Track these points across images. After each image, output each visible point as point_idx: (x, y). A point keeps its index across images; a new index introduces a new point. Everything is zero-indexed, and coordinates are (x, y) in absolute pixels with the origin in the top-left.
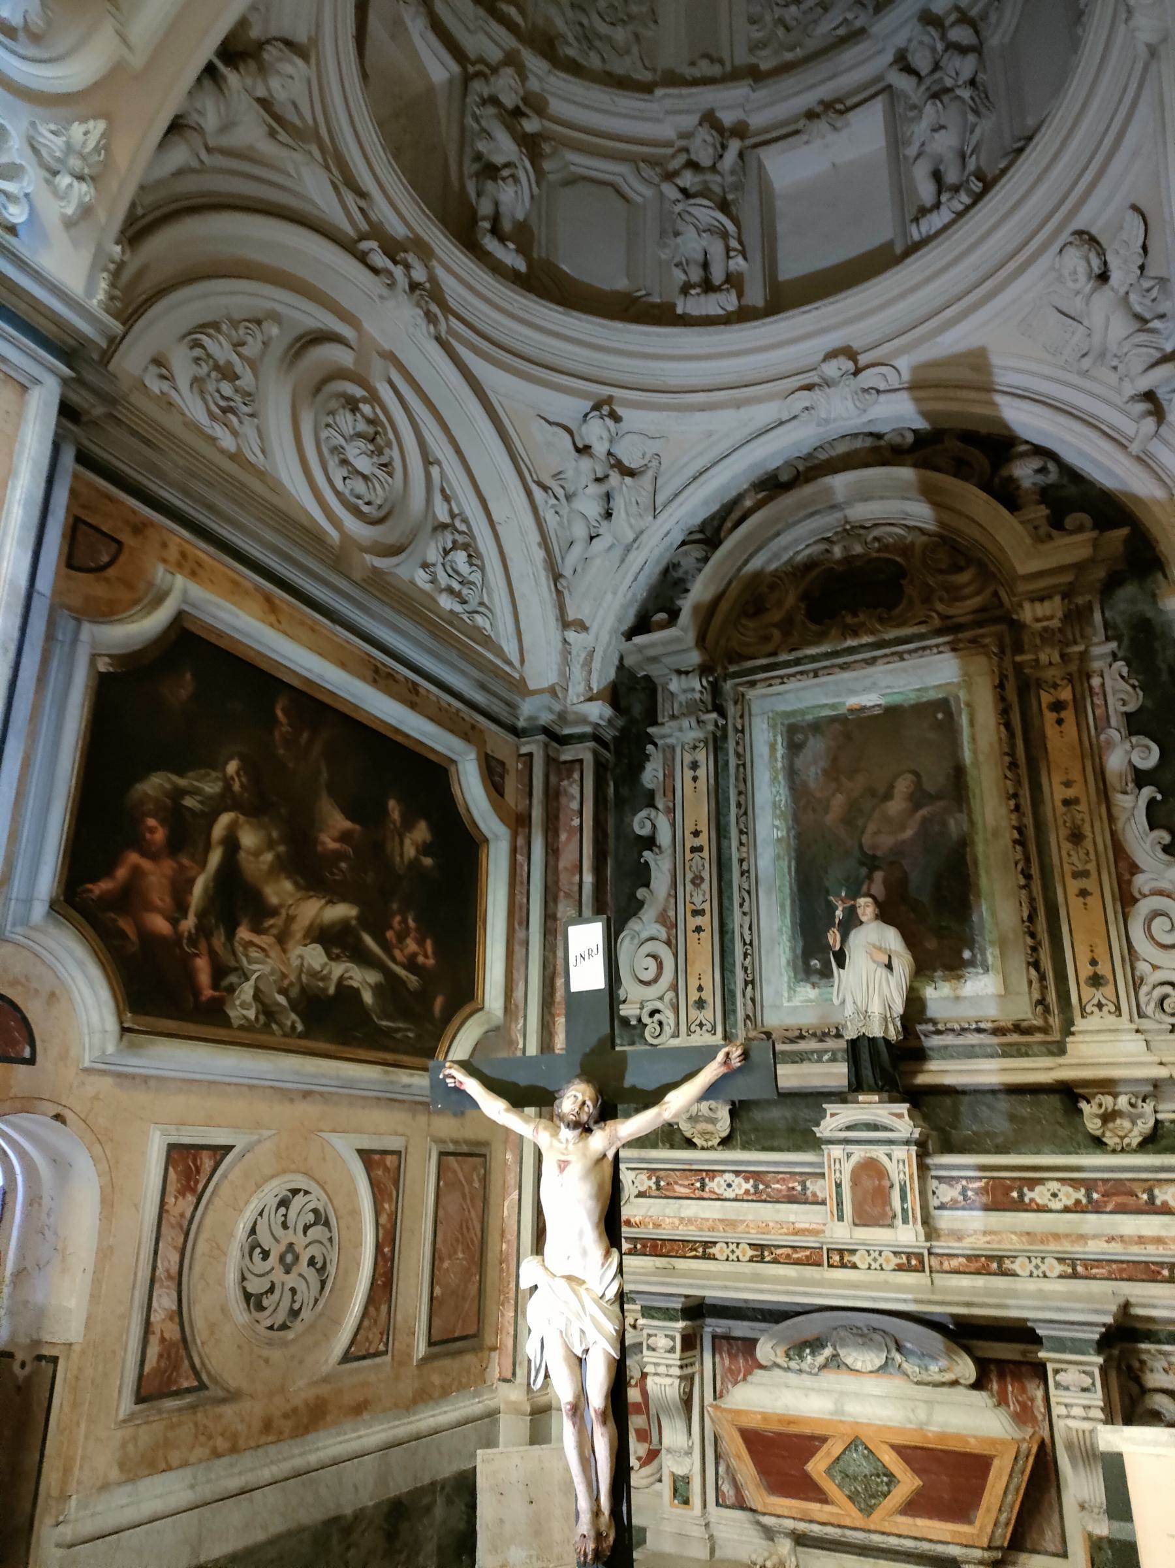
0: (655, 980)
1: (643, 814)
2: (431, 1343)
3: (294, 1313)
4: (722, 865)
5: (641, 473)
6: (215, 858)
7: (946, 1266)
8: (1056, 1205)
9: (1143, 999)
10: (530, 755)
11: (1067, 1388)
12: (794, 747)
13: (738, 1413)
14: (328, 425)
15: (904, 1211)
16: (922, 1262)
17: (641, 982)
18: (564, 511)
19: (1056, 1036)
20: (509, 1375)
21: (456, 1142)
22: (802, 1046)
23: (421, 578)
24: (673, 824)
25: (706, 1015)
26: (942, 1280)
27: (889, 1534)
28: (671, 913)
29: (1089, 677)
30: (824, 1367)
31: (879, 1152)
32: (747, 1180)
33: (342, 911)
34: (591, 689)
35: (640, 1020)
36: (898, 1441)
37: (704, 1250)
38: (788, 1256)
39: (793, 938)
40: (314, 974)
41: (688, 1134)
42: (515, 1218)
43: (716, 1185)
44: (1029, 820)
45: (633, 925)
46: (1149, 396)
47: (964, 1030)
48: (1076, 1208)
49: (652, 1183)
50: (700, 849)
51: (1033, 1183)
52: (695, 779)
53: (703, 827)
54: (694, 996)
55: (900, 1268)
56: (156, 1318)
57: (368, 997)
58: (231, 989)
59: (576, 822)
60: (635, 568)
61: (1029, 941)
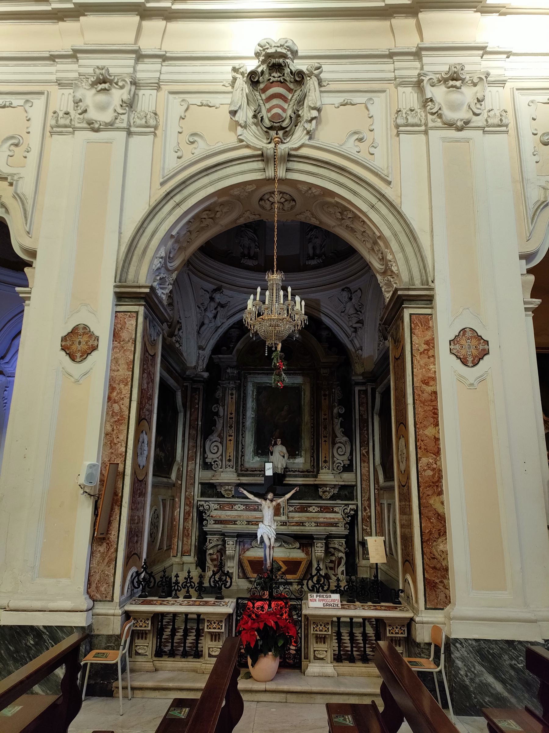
0: (216, 453)
1: (215, 405)
4: (238, 423)
5: (226, 306)
7: (291, 525)
8: (314, 511)
9: (334, 466)
10: (187, 386)
12: (259, 393)
15: (283, 513)
17: (212, 453)
19: (315, 473)
20: (176, 555)
22: (255, 472)
24: (224, 410)
25: (231, 463)
26: (290, 527)
28: (222, 435)
29: (332, 389)
32: (244, 506)
35: (211, 463)
37: (234, 522)
39: (254, 444)
41: (223, 494)
43: (236, 507)
45: (211, 437)
46: (355, 328)
47: (295, 471)
50: (232, 418)
52: (232, 398)
53: (234, 412)
55: (281, 525)
61: (312, 451)
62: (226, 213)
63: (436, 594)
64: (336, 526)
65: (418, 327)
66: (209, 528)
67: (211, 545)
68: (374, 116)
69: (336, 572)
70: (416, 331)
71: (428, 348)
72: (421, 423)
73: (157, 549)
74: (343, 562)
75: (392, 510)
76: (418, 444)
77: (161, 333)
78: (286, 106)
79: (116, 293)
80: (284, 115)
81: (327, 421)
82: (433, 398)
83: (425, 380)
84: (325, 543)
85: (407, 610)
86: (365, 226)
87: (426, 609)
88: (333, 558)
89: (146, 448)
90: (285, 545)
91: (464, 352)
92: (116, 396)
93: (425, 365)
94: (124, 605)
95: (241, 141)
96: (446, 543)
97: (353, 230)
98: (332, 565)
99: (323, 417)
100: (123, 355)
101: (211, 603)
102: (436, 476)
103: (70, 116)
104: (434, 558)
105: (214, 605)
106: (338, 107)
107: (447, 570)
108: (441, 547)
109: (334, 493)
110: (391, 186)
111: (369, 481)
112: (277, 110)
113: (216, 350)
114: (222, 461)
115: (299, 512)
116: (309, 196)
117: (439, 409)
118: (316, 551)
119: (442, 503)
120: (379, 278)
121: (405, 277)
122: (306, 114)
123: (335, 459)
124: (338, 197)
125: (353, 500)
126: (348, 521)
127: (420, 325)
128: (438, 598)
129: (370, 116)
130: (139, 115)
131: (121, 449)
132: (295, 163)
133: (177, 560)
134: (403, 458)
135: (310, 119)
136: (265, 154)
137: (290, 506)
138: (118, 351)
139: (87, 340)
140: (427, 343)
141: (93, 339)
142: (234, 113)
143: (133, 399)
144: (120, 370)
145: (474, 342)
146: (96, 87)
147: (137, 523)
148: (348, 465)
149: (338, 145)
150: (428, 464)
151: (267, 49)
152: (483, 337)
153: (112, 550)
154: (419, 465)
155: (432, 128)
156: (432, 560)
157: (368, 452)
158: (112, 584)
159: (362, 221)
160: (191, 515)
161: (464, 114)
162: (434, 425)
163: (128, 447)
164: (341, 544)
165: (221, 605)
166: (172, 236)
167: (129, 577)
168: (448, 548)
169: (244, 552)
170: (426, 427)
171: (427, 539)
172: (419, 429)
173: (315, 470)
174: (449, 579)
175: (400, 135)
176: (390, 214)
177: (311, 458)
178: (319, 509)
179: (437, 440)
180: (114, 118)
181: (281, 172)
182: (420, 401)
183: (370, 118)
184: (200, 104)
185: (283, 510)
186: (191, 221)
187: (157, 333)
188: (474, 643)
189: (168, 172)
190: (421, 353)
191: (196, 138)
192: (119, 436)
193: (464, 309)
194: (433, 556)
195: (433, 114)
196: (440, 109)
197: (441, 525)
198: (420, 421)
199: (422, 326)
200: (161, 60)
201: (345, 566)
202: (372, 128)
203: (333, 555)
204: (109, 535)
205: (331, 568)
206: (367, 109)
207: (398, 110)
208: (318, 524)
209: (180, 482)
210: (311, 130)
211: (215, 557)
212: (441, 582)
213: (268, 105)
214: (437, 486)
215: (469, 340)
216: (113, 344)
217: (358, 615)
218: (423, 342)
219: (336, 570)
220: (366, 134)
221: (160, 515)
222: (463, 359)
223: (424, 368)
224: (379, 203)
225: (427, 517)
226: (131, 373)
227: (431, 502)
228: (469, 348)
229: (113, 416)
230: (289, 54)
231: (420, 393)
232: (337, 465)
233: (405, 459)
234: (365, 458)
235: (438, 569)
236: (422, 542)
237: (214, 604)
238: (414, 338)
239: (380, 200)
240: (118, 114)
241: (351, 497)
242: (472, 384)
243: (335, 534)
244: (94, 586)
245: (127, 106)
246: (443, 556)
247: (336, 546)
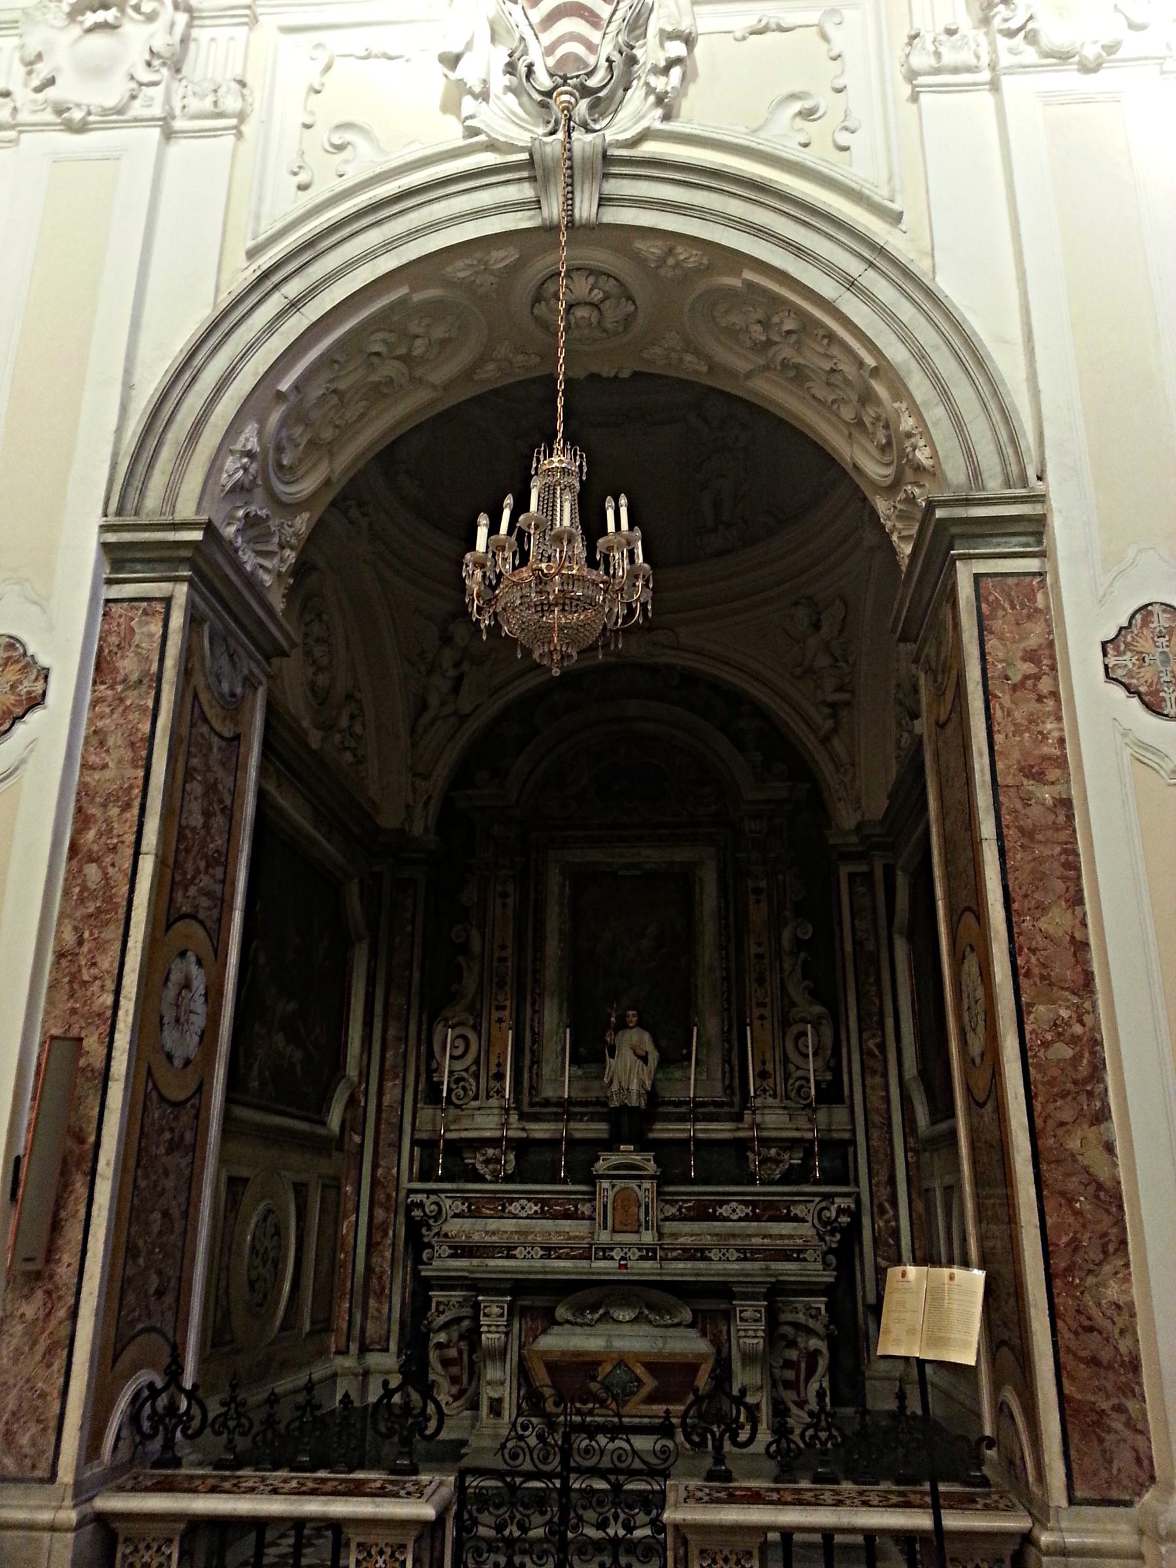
2: (313, 1322)
7: (670, 1256)
8: (735, 1217)
9: (789, 1088)
11: (746, 1321)
13: (545, 1352)
15: (647, 1222)
16: (655, 1254)
19: (736, 1110)
27: (634, 1416)
28: (478, 1006)
30: (599, 1320)
31: (633, 1184)
36: (648, 1359)
38: (567, 1254)
42: (352, 1234)
44: (733, 965)
48: (746, 1218)
49: (465, 1207)
50: (504, 960)
51: (721, 1203)
52: (504, 905)
54: (494, 1070)
61: (726, 1046)
62: (443, 343)
63: (1104, 1451)
64: (798, 1259)
65: (1000, 613)
66: (437, 1270)
67: (442, 1319)
68: (847, 56)
69: (802, 1395)
70: (997, 625)
71: (1036, 670)
72: (1026, 896)
73: (276, 1330)
74: (823, 1364)
75: (955, 1213)
77: (261, 683)
78: (595, 36)
79: (105, 547)
80: (592, 60)
81: (766, 961)
82: (1062, 819)
83: (1032, 767)
84: (767, 1309)
85: (1009, 1508)
86: (835, 351)
87: (1072, 1501)
88: (793, 1355)
89: (199, 1005)
90: (651, 1317)
91: (1148, 676)
92: (94, 842)
93: (1030, 722)
94: (90, 1494)
95: (473, 132)
96: (1127, 1279)
97: (798, 376)
98: (790, 1375)
99: (754, 950)
100: (122, 721)
101: (373, 1485)
102: (1085, 1061)
103: (14, 101)
104: (1091, 1329)
105: (381, 1493)
106: (744, 38)
107: (1134, 1366)
108: (1112, 1291)
109: (791, 1165)
110: (903, 227)
111: (890, 1126)
113: (461, 777)
114: (477, 1076)
115: (691, 1219)
116: (669, 275)
117: (1081, 851)
118: (742, 1333)
119: (1109, 1148)
120: (882, 505)
121: (955, 472)
122: (650, 52)
123: (792, 1068)
124: (752, 269)
125: (846, 1183)
126: (834, 1245)
127: (1007, 606)
128: (1110, 1462)
129: (834, 53)
130: (197, 89)
131: (101, 1000)
133: (348, 1362)
134: (977, 1015)
135: (662, 64)
136: (536, 157)
137: (666, 1202)
138: (108, 710)
139: (14, 678)
140: (1031, 656)
141: (33, 677)
142: (452, 61)
143: (144, 848)
144: (111, 764)
146: (80, 18)
147: (160, 1234)
148: (829, 1083)
149: (745, 130)
150: (1055, 1025)
153: (62, 1313)
155: (1011, 70)
157: (882, 1046)
158: (53, 1424)
159: (824, 337)
160: (391, 1233)
162: (1067, 901)
163: (124, 992)
164: (814, 1312)
165: (402, 1493)
166: (280, 396)
167: (123, 1402)
168: (1134, 1291)
169: (536, 1337)
170: (1042, 909)
171: (1063, 1265)
172: (1019, 915)
173: (737, 1099)
174: (1144, 1397)
175: (922, 96)
176: (904, 300)
177: (723, 1066)
178: (749, 1210)
179: (1080, 947)
180: (127, 95)
181: (586, 205)
183: (834, 59)
184: (364, 53)
185: (647, 1214)
186: (337, 357)
187: (246, 679)
189: (267, 229)
190: (1014, 688)
191: (348, 136)
192: (98, 959)
193: (1140, 551)
194: (1086, 1323)
195: (1011, 34)
197: (1107, 1220)
198: (1023, 891)
199: (1013, 607)
201: (827, 1377)
202: (839, 84)
203: (792, 1344)
204: (53, 1266)
205: (788, 1385)
206: (825, 37)
207: (913, 33)
208: (746, 1254)
209: (357, 1139)
210: (666, 92)
211: (453, 1353)
212: (1120, 1409)
213: (548, 38)
214: (1090, 1094)
215: (1161, 639)
216: (94, 691)
217: (846, 1526)
219: (802, 1389)
220: (824, 100)
221: (287, 1228)
222: (1147, 694)
223: (1028, 729)
224: (871, 273)
226: (142, 774)
227: (1073, 1144)
229: (82, 900)
232: (798, 1083)
233: (981, 1017)
234: (874, 1064)
235: (1105, 1363)
237: (382, 1488)
238: (992, 643)
239: (871, 264)
240: (141, 84)
241: (841, 1175)
243: (791, 1282)
245: (164, 64)
246: (1120, 1322)
247: (801, 1318)
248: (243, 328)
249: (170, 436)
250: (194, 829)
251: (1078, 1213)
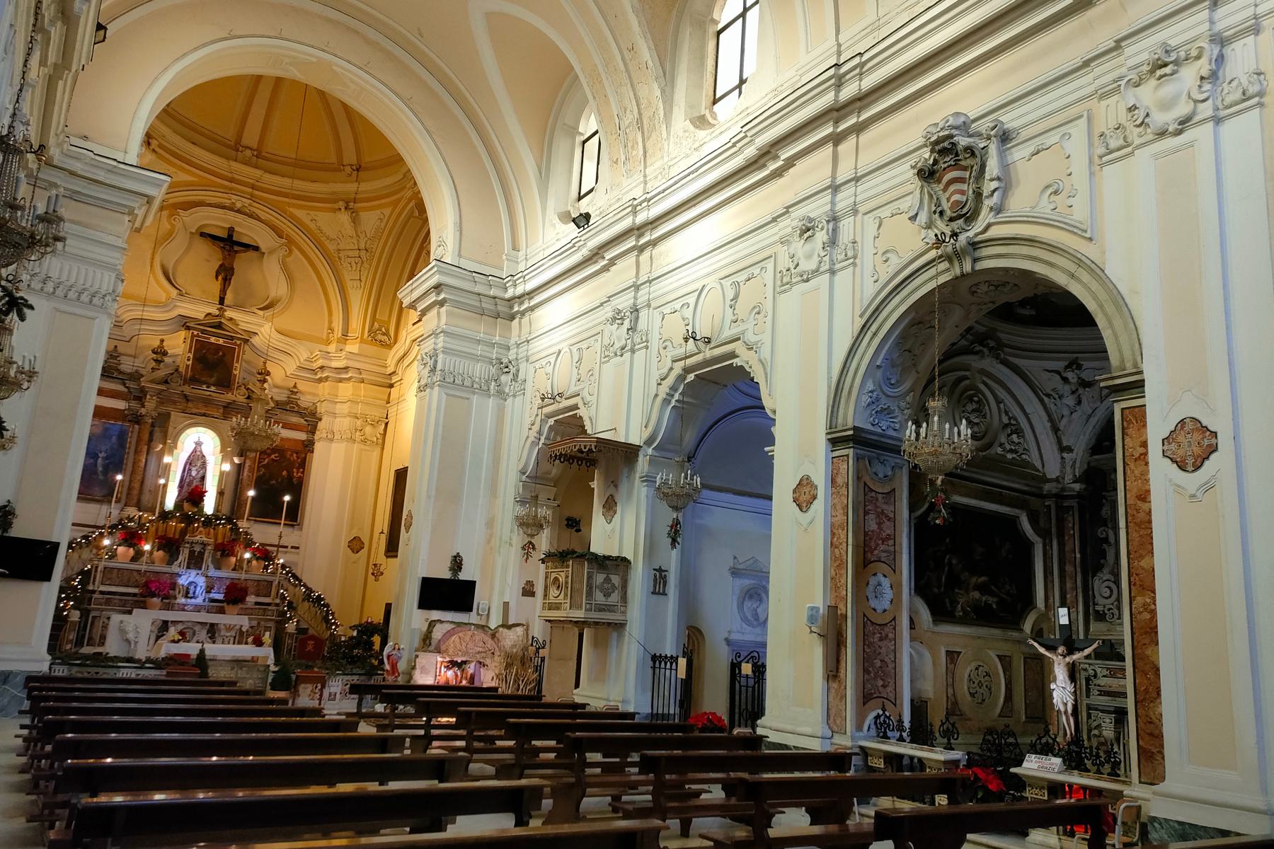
0: (1110, 597)
1: (1102, 529)
2: (1026, 717)
3: (984, 700)
6: (946, 569)
10: (1050, 505)
14: (963, 412)
18: (1059, 404)
21: (1030, 654)
23: (999, 450)
33: (983, 579)
34: (1076, 476)
35: (1104, 611)
40: (976, 600)
56: (949, 695)
57: (994, 606)
58: (955, 607)
59: (1072, 532)
60: (1093, 424)
65: (1132, 425)
70: (1130, 431)
76: (1132, 579)
78: (965, 187)
104: (1151, 723)
112: (956, 197)
132: (984, 249)
145: (1197, 436)
151: (930, 138)
152: (1209, 428)
153: (843, 687)
154: (1133, 606)
156: (1148, 724)
161: (1183, 109)
166: (879, 367)
182: (1135, 523)
188: (1176, 825)
190: (1136, 460)
196: (1148, 115)
200: (854, 182)
213: (947, 194)
218: (1139, 444)
223: (1140, 479)
225: (1143, 671)
228: (1190, 446)
230: (954, 132)
231: (1135, 513)
236: (1136, 702)
238: (1128, 440)
242: (1193, 496)
244: (832, 718)
248: (860, 348)
249: (843, 394)
250: (873, 531)
251: (1149, 679)
